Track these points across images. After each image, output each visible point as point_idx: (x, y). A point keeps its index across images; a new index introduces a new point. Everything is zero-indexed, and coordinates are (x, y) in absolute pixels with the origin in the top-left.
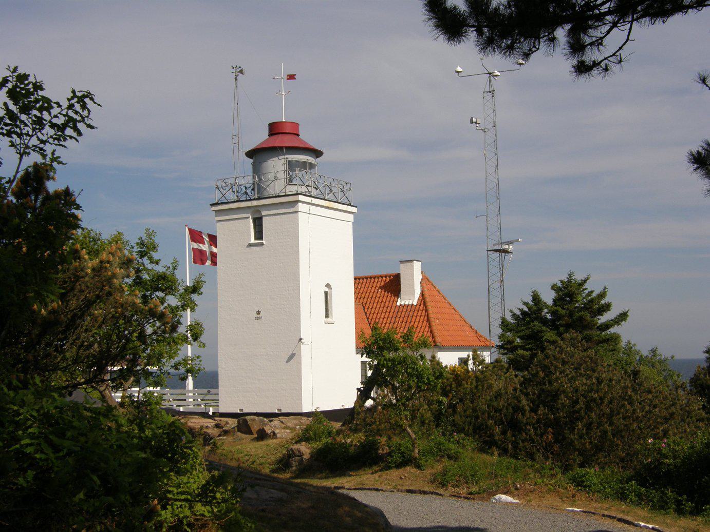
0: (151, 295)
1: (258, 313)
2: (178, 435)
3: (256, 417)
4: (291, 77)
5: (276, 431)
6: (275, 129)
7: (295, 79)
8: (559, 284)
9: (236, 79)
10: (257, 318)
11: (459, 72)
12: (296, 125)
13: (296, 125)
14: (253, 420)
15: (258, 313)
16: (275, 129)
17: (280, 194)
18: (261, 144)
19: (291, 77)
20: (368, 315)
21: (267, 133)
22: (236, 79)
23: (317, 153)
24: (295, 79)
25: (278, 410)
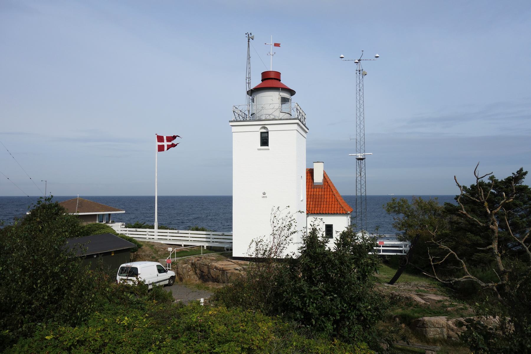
0: (441, 237)
1: (264, 194)
2: (340, 351)
4: (277, 45)
6: (266, 76)
7: (280, 46)
8: (469, 187)
9: (249, 41)
11: (342, 58)
12: (278, 74)
13: (278, 74)
15: (264, 194)
16: (266, 76)
17: (282, 118)
18: (257, 86)
19: (277, 45)
20: (333, 197)
21: (260, 78)
22: (249, 41)
23: (292, 92)
24: (280, 46)
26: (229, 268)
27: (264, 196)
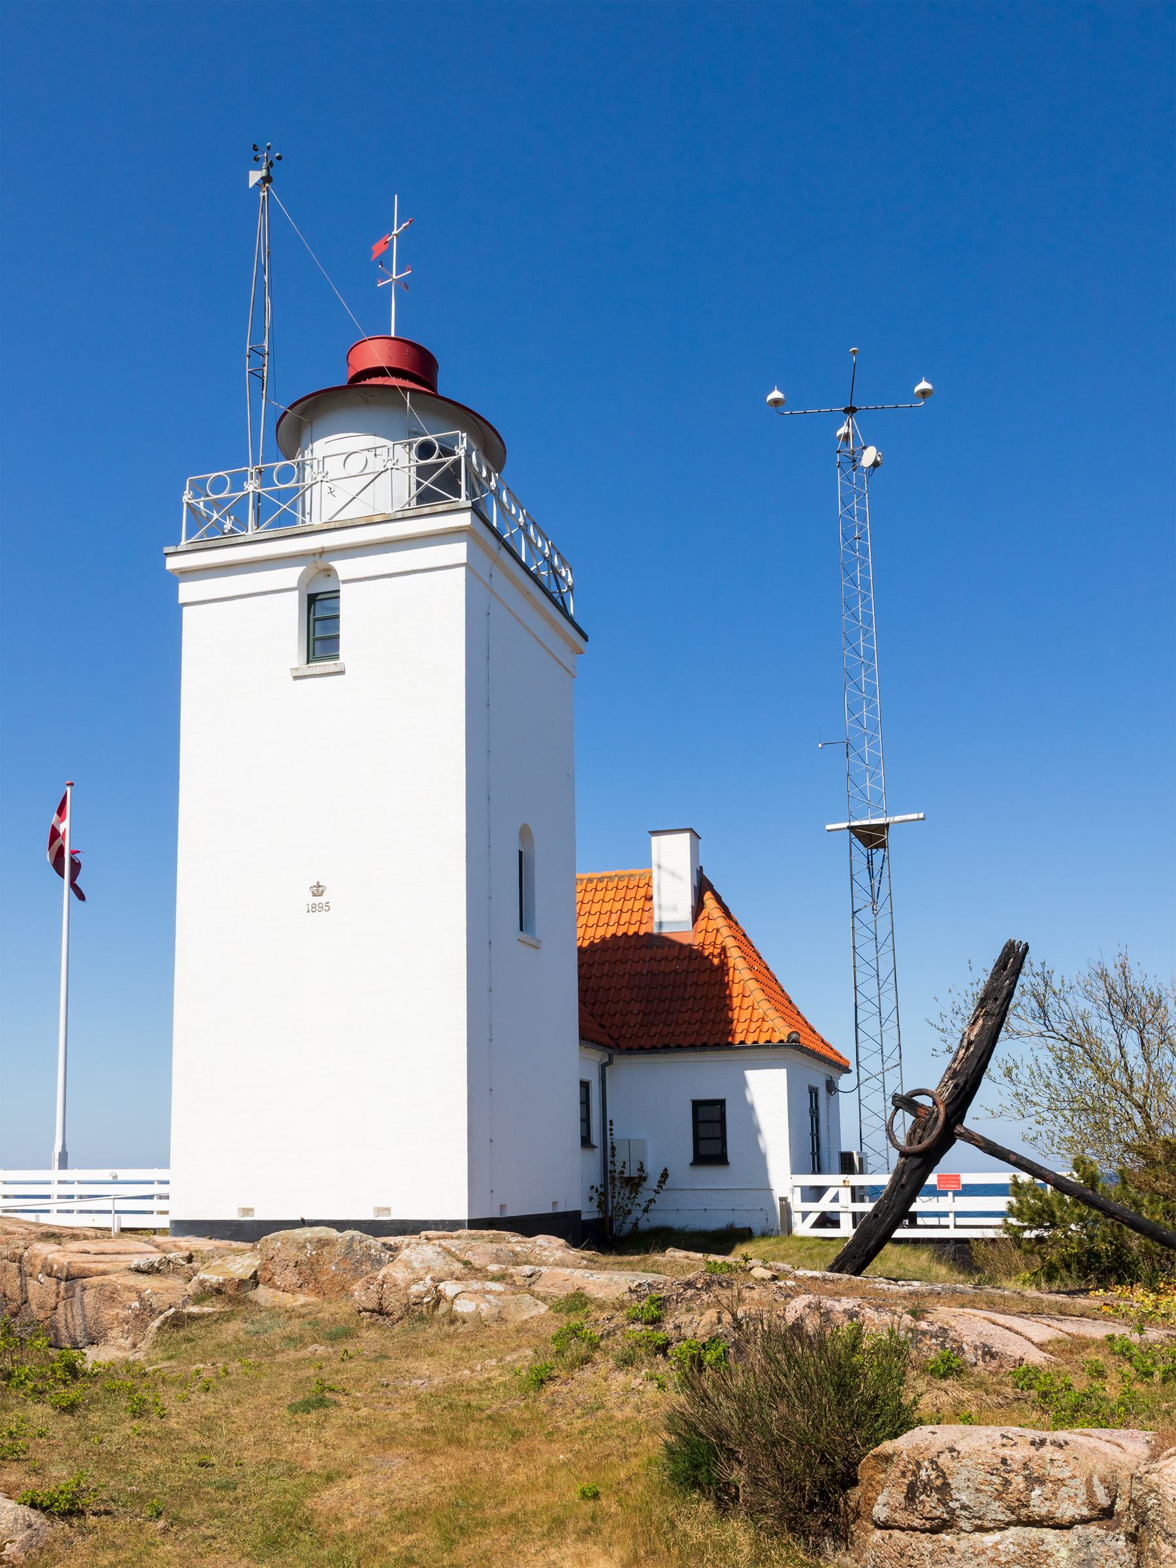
1: (318, 890)
3: (333, 1233)
5: (449, 1288)
10: (314, 908)
14: (322, 1243)
15: (318, 890)
25: (379, 1210)
26: (101, 1267)
27: (317, 900)
